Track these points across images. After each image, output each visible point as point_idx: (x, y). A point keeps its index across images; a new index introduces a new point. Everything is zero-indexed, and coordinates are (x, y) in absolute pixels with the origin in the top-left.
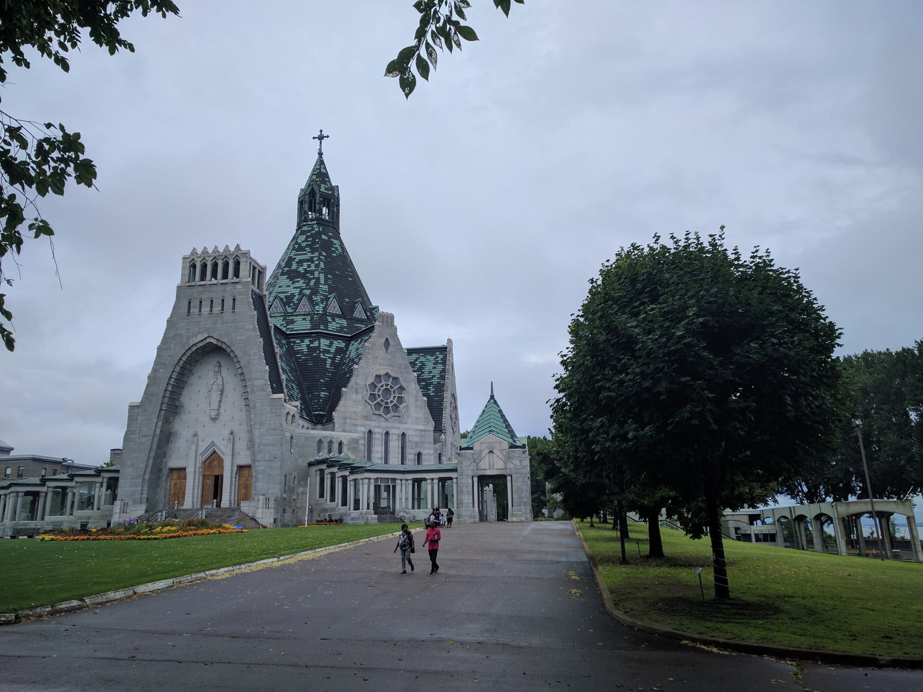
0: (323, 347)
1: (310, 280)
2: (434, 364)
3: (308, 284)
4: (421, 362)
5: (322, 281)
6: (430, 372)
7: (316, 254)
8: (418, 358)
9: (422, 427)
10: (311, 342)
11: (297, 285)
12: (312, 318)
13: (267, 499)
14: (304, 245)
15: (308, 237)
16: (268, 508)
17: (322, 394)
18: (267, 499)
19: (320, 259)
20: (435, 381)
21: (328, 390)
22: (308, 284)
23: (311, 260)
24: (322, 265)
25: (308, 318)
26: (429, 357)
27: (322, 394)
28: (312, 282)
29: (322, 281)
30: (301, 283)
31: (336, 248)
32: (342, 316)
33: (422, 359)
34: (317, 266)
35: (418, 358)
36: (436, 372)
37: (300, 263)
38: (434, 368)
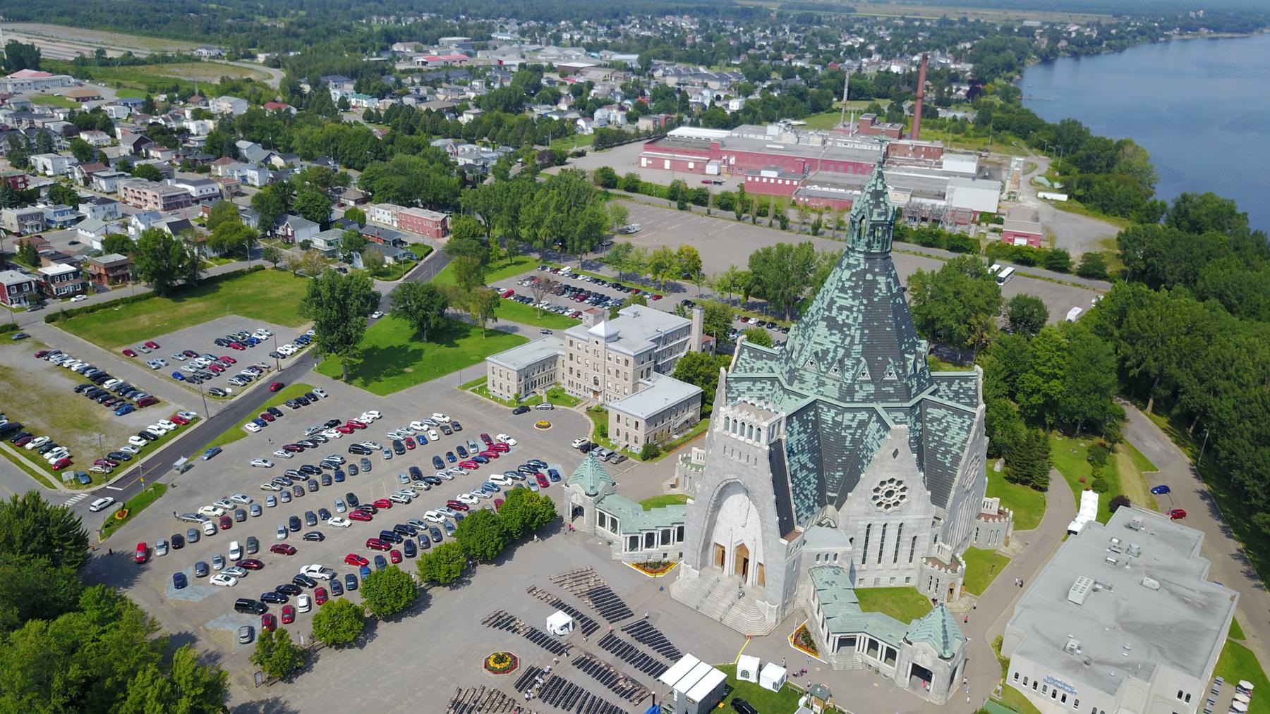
0: (846, 423)
1: (846, 336)
2: (960, 429)
3: (843, 340)
4: (948, 422)
5: (857, 341)
6: (953, 438)
7: (857, 303)
8: (946, 416)
9: (922, 517)
10: (837, 414)
11: (833, 338)
12: (841, 385)
13: (934, 581)
14: (848, 284)
15: (853, 274)
16: (504, 697)
17: (838, 475)
18: (934, 581)
19: (859, 311)
20: (955, 450)
21: (844, 470)
22: (843, 340)
23: (850, 309)
24: (860, 319)
25: (838, 384)
26: (956, 418)
27: (838, 475)
28: (848, 339)
29: (857, 341)
30: (837, 338)
31: (880, 290)
32: (872, 381)
33: (949, 418)
34: (855, 319)
35: (946, 416)
36: (958, 440)
37: (841, 308)
38: (958, 434)
